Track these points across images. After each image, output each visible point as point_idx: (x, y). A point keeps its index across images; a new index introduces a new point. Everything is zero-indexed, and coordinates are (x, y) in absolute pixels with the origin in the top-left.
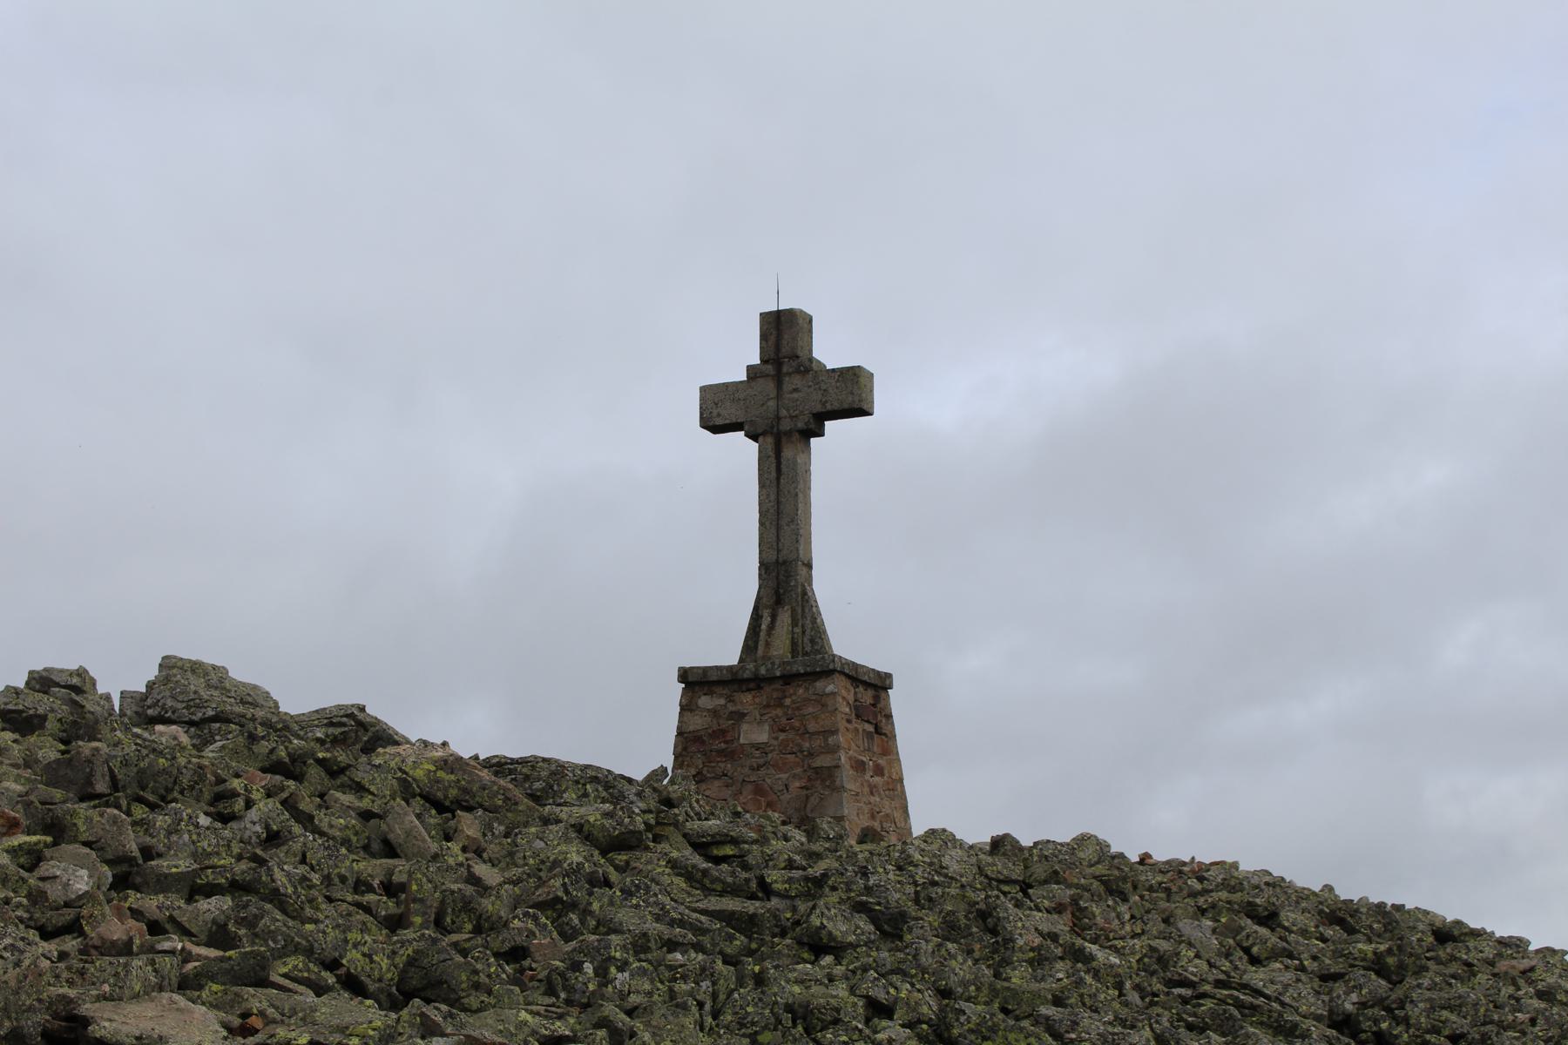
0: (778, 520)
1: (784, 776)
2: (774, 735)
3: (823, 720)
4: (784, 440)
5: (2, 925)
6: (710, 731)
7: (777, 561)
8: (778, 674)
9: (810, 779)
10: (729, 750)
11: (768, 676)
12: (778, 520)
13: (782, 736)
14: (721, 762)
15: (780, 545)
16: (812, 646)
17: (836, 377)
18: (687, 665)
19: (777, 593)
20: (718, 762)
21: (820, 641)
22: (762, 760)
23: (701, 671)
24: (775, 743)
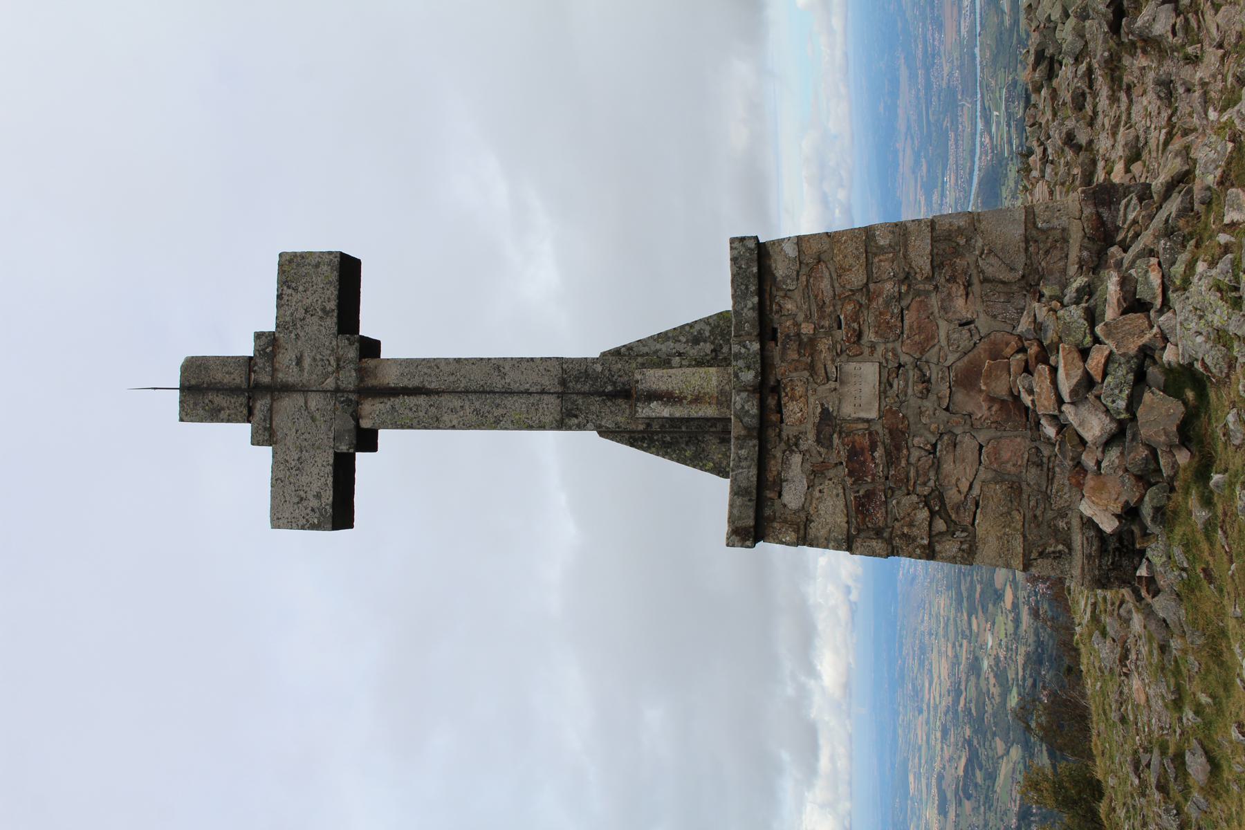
0: (495, 393)
1: (943, 327)
2: (867, 351)
3: (845, 257)
4: (371, 382)
6: (849, 481)
7: (560, 395)
8: (756, 346)
9: (952, 279)
10: (888, 441)
11: (758, 366)
12: (495, 393)
13: (870, 336)
14: (908, 457)
15: (533, 389)
16: (705, 341)
17: (290, 291)
18: (724, 528)
19: (613, 396)
20: (908, 463)
22: (911, 373)
23: (738, 501)
24: (880, 349)
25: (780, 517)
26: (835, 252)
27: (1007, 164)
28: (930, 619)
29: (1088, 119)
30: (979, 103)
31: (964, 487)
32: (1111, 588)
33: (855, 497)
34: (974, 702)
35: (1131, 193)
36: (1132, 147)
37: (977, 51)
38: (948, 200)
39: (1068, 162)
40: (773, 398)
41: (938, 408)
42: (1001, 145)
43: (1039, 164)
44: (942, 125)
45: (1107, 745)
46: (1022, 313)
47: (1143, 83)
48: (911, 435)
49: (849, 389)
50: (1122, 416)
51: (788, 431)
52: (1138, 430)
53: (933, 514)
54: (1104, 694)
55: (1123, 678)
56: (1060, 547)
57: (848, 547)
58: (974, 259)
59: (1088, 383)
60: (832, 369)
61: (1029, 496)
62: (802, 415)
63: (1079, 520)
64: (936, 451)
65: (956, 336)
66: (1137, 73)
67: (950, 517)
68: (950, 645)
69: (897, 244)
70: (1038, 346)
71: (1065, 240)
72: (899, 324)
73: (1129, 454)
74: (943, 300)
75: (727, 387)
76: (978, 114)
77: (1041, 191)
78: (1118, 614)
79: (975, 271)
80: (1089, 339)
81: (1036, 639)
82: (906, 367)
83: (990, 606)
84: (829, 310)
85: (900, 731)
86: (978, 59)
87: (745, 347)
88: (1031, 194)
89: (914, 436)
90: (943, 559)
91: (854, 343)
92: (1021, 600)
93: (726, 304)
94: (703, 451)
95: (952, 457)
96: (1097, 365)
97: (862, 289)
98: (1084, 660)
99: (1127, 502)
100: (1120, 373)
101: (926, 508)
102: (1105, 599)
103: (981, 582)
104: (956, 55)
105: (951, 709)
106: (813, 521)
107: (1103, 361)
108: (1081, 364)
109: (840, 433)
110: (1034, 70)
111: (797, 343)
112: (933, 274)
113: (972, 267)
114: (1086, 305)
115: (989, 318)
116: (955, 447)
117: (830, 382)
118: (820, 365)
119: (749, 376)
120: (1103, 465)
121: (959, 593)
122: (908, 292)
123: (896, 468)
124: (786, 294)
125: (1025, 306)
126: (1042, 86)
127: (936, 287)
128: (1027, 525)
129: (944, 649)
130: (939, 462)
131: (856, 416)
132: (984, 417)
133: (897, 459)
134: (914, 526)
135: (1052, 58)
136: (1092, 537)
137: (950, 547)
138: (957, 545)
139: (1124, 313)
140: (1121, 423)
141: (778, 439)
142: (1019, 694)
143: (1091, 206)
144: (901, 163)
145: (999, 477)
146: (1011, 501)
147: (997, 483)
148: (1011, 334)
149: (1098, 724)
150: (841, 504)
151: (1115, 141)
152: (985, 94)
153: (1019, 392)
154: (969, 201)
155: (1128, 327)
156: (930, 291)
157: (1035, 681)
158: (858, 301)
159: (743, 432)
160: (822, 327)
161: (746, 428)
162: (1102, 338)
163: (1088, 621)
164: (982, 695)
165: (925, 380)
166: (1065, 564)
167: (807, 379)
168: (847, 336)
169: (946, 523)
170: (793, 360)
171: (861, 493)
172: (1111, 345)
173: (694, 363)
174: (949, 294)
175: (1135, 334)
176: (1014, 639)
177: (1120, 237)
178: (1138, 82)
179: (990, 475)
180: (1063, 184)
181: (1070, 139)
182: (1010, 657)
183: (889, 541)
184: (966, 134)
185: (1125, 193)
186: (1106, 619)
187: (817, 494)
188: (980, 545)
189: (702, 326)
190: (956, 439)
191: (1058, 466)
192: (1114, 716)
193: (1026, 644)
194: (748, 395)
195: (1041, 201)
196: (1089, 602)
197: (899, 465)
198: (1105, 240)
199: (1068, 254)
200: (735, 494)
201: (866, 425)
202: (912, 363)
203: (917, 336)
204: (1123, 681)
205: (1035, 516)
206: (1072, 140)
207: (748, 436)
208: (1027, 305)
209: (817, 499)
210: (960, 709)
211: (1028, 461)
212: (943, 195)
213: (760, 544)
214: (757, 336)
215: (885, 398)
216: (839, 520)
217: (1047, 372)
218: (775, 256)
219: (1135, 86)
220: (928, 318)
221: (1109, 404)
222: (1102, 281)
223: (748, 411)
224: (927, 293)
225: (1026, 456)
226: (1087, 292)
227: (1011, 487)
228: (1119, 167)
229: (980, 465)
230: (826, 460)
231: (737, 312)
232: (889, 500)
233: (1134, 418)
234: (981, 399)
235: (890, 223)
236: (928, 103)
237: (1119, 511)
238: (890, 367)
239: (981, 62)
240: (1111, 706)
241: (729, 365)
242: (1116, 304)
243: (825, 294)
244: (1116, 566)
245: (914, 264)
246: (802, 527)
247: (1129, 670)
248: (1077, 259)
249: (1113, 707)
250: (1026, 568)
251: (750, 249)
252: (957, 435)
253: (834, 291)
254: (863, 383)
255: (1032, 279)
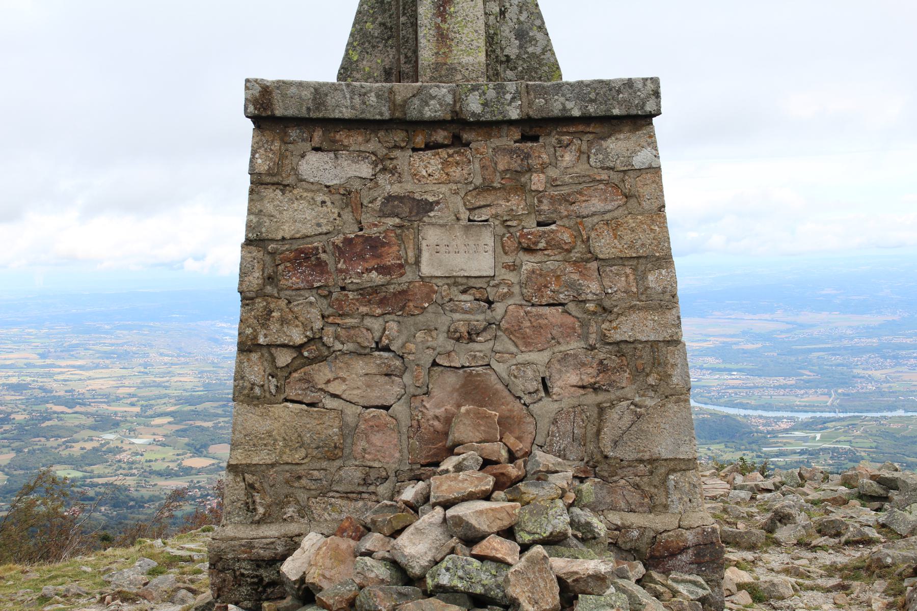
1: (540, 358)
2: (509, 259)
6: (338, 240)
9: (603, 368)
11: (488, 117)
13: (529, 263)
16: (521, 47)
18: (270, 75)
20: (363, 316)
22: (481, 317)
23: (307, 94)
24: (511, 277)
25: (287, 150)
26: (639, 217)
27: (752, 451)
28: (165, 364)
29: (807, 540)
30: (832, 415)
31: (334, 388)
32: (211, 574)
33: (317, 248)
34: (60, 423)
35: (712, 588)
36: (770, 592)
37: (900, 413)
38: (708, 377)
39: (752, 516)
40: (445, 138)
41: (436, 352)
42: (777, 442)
43: (752, 484)
44: (805, 369)
45: (11, 582)
46: (559, 457)
47: (850, 604)
48: (400, 319)
49: (459, 238)
50: (429, 581)
51: (402, 159)
52: (412, 600)
53: (299, 348)
54: (76, 575)
55: (98, 597)
56: (261, 510)
57: (251, 241)
58: (629, 396)
59: (471, 539)
60: (485, 214)
61: (325, 470)
62: (424, 177)
63: (297, 532)
64: (380, 350)
65: (530, 373)
66: (864, 597)
67: (295, 371)
68: (132, 390)
69: (649, 299)
70: (518, 477)
71: (652, 509)
72: (544, 302)
73: (381, 590)
74: (575, 356)
75: (459, 77)
76: (818, 415)
77: (718, 486)
78: (179, 588)
79: (613, 397)
80: (527, 538)
81: (147, 498)
82: (489, 311)
83: (186, 440)
84: (563, 211)
85: (15, 330)
86: (889, 414)
87: (513, 99)
88: (713, 474)
89: (399, 322)
90: (240, 363)
91: (520, 243)
92: (195, 479)
93: (570, 74)
94: (373, 47)
95: (373, 372)
96: (494, 548)
97: (590, 252)
98: (119, 552)
99: (321, 589)
100: (483, 576)
101: (305, 340)
102: (199, 572)
103: (215, 427)
104: (896, 386)
105: (49, 395)
106: (284, 194)
107: (499, 556)
108: (495, 530)
109: (401, 227)
110: (873, 477)
111: (519, 169)
112: (610, 344)
113: (618, 393)
114: (570, 535)
115: (553, 415)
116: (386, 375)
117: (468, 213)
118: (489, 198)
119: (474, 105)
120: (367, 558)
121: (200, 400)
122: (586, 311)
123: (357, 300)
124: (583, 153)
125: (568, 460)
126: (851, 487)
127: (592, 348)
128: (287, 467)
129: (127, 384)
130: (365, 355)
131: (424, 247)
132: (425, 411)
133: (369, 301)
134: (282, 325)
135: (886, 499)
136: (275, 549)
137: (256, 372)
138: (259, 381)
139: (560, 580)
140: (421, 579)
141: (390, 145)
142: (73, 480)
143: (695, 540)
144: (757, 317)
145: (349, 432)
146: (317, 448)
147: (341, 428)
148: (533, 443)
149: (37, 571)
150: (308, 229)
151: (778, 572)
152: (845, 423)
153: (459, 454)
154: (706, 404)
155: (542, 585)
156: (587, 340)
157: (92, 499)
158: (574, 248)
159: (399, 99)
160: (540, 201)
161: (405, 101)
162: (528, 554)
163: (169, 553)
164: (69, 434)
165: (471, 336)
166: (239, 516)
167: (471, 182)
168: (529, 234)
169: (287, 366)
170: (496, 164)
171: (323, 256)
172: (519, 564)
173: (492, 32)
174: (583, 365)
175: (533, 593)
176: (145, 471)
177: (655, 575)
178: (852, 599)
179: (350, 420)
180: (725, 510)
181: (782, 518)
182: (121, 468)
183: (260, 293)
184: (792, 398)
185: (711, 581)
186: (172, 575)
187: (320, 198)
188: (258, 410)
189: (542, 43)
190: (395, 375)
191: (365, 505)
192: (48, 589)
193: (139, 485)
194: (449, 104)
195: (704, 487)
196: (194, 553)
197: (362, 304)
198: (652, 557)
199: (635, 512)
200: (316, 90)
201: (411, 260)
202: (494, 317)
203: (528, 324)
204: (94, 597)
205: (300, 478)
206: (780, 521)
207: (394, 106)
208: (570, 463)
209: (313, 199)
210: (49, 406)
211: (370, 467)
212: (714, 370)
213: (250, 125)
214: (528, 115)
215: (448, 284)
216: (286, 227)
217: (483, 488)
218: (634, 139)
219: (847, 595)
220: (553, 338)
221: (444, 564)
222: (600, 554)
223: (427, 104)
224: (585, 337)
225: (376, 464)
226: (587, 537)
227: (335, 447)
228: (745, 577)
229: (363, 407)
230: (364, 209)
231: (559, 87)
232: (314, 292)
233: (427, 594)
234: (448, 407)
235: (676, 288)
236: (834, 351)
237: (309, 579)
238: (489, 289)
239: (885, 418)
240: (62, 584)
241: (489, 79)
242: (572, 570)
243: (584, 205)
244: (239, 579)
245: (623, 318)
246: (275, 179)
247: (108, 603)
248: (628, 523)
249: (60, 587)
250: (233, 468)
251: (644, 104)
252: (401, 377)
253: (588, 216)
254: (467, 255)
255: (603, 470)
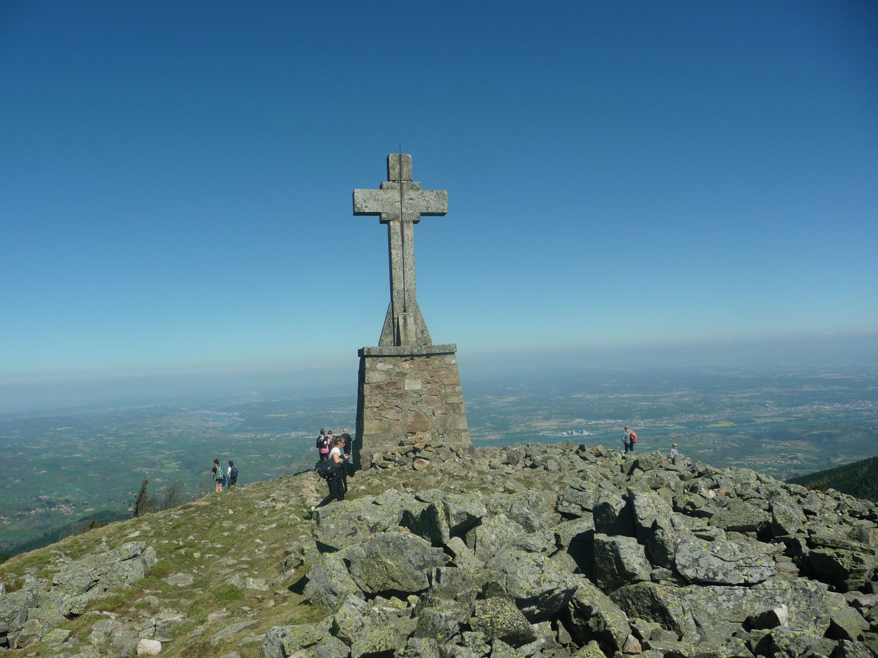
5: (1, 578)
6: (386, 382)
8: (425, 353)
13: (429, 386)
16: (422, 335)
17: (434, 195)
21: (426, 332)
24: (425, 390)
